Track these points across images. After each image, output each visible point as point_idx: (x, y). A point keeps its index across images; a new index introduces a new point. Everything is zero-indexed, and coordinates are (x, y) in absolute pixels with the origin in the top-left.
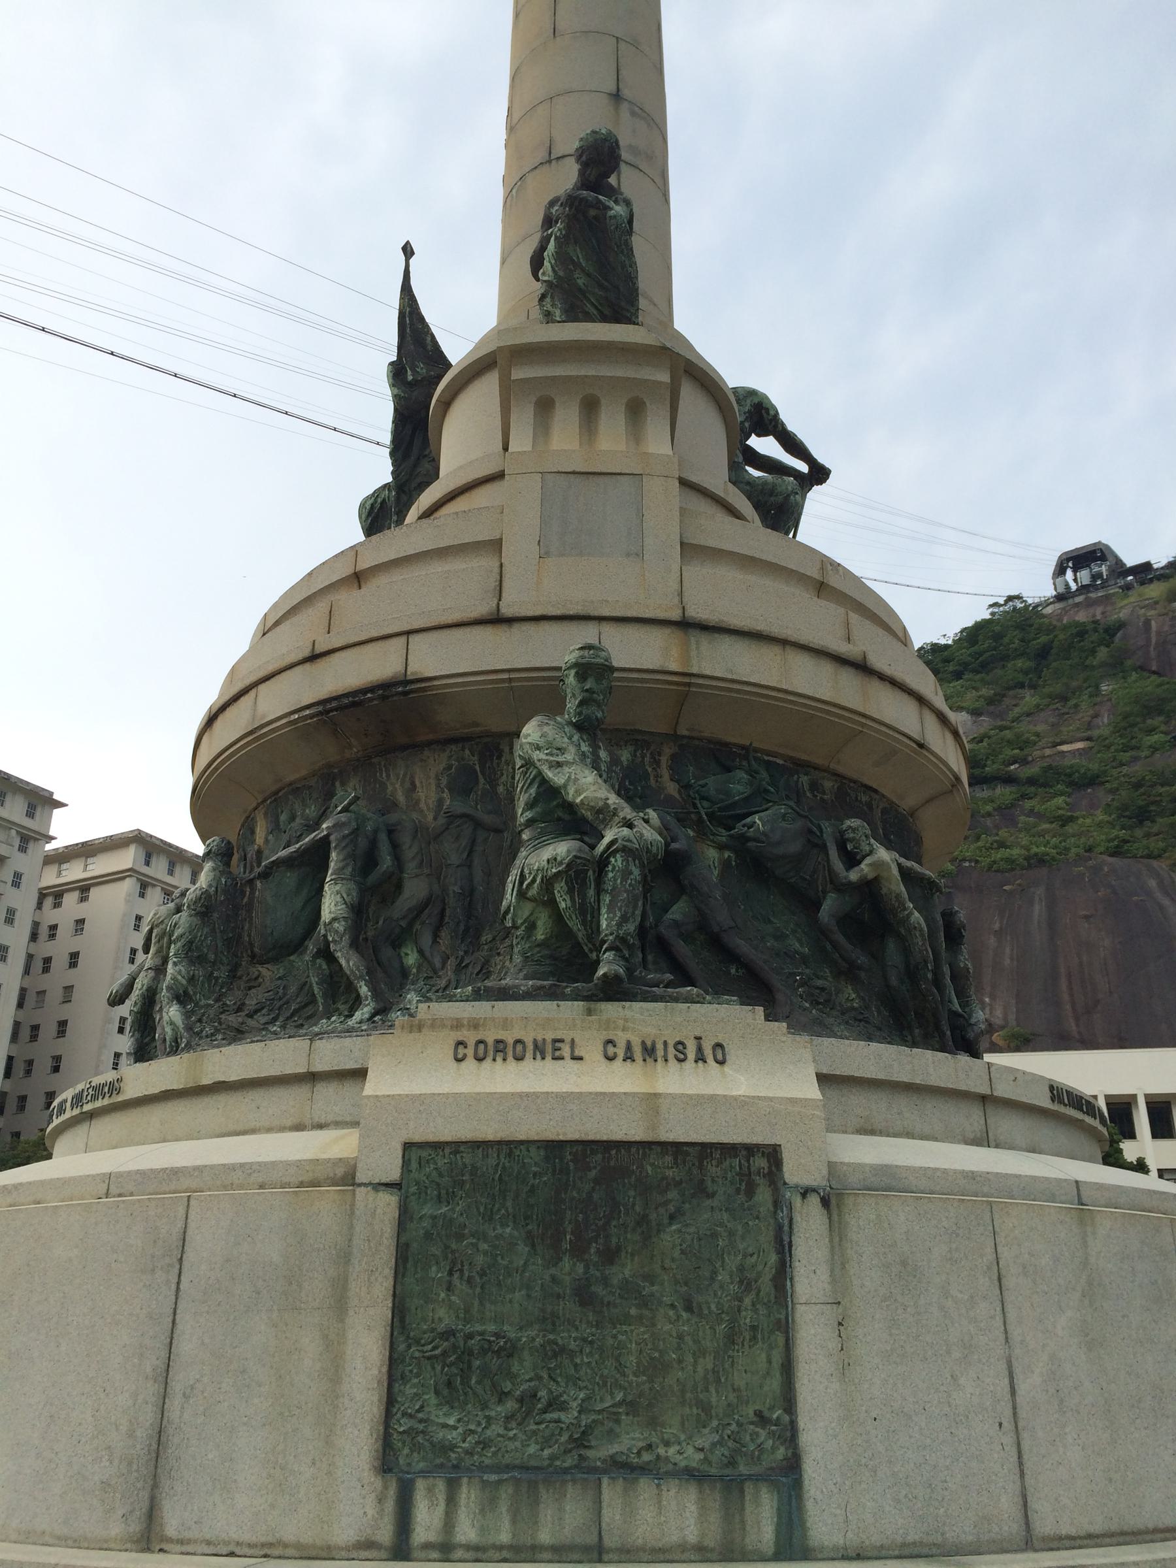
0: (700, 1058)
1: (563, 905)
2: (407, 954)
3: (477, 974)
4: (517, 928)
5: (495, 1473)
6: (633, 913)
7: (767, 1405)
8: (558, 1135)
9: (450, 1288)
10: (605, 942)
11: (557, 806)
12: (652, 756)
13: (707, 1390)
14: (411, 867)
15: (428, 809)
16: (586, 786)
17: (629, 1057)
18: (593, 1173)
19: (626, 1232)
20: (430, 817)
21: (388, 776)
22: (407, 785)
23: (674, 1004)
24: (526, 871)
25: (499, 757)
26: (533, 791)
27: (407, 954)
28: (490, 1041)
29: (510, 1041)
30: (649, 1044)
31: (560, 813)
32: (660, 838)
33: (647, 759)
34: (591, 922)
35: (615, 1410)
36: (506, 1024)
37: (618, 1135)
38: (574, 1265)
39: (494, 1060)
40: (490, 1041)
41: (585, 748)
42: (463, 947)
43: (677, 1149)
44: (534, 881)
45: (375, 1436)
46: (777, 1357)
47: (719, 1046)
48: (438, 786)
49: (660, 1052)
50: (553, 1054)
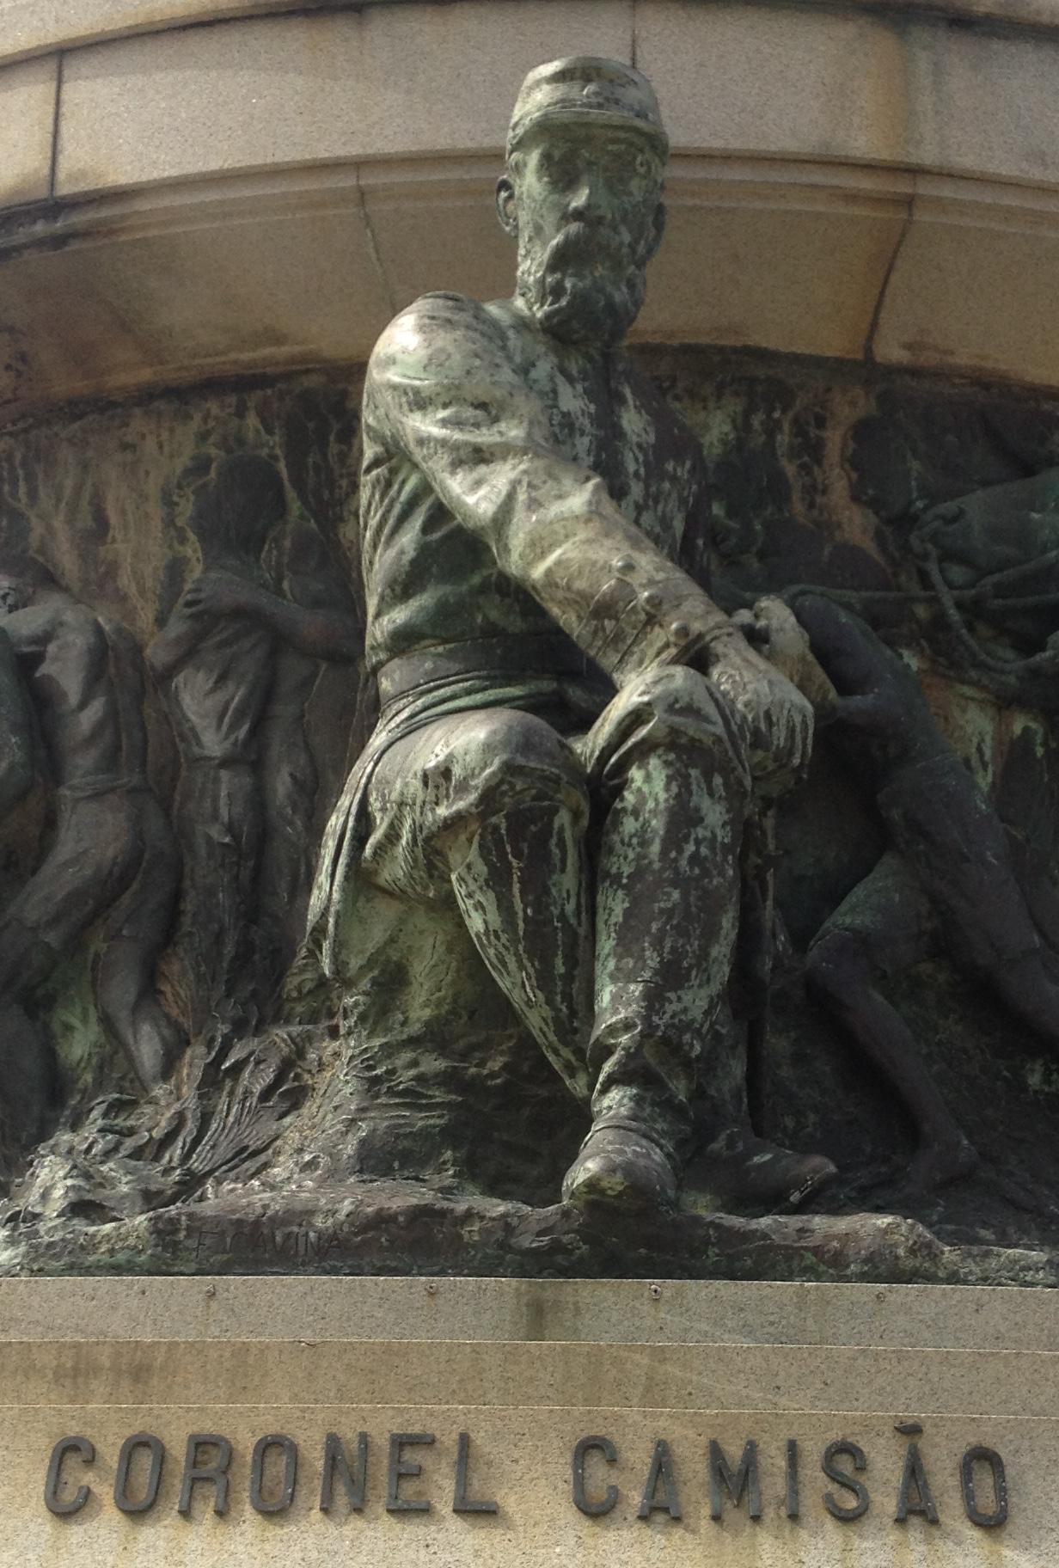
0: (917, 1508)
1: (476, 923)
2: (69, 1028)
3: (265, 1095)
4: (348, 984)
6: (703, 955)
10: (609, 1051)
11: (483, 589)
12: (799, 428)
14: (82, 765)
15: (142, 592)
16: (561, 533)
17: (661, 1508)
20: (146, 616)
21: (33, 495)
22: (86, 521)
24: (375, 804)
26: (409, 539)
27: (69, 1028)
29: (246, 1443)
30: (734, 1451)
31: (493, 611)
32: (798, 698)
33: (783, 439)
34: (568, 978)
36: (242, 1370)
41: (572, 401)
42: (231, 1010)
47: (982, 1458)
48: (170, 522)
49: (773, 1483)
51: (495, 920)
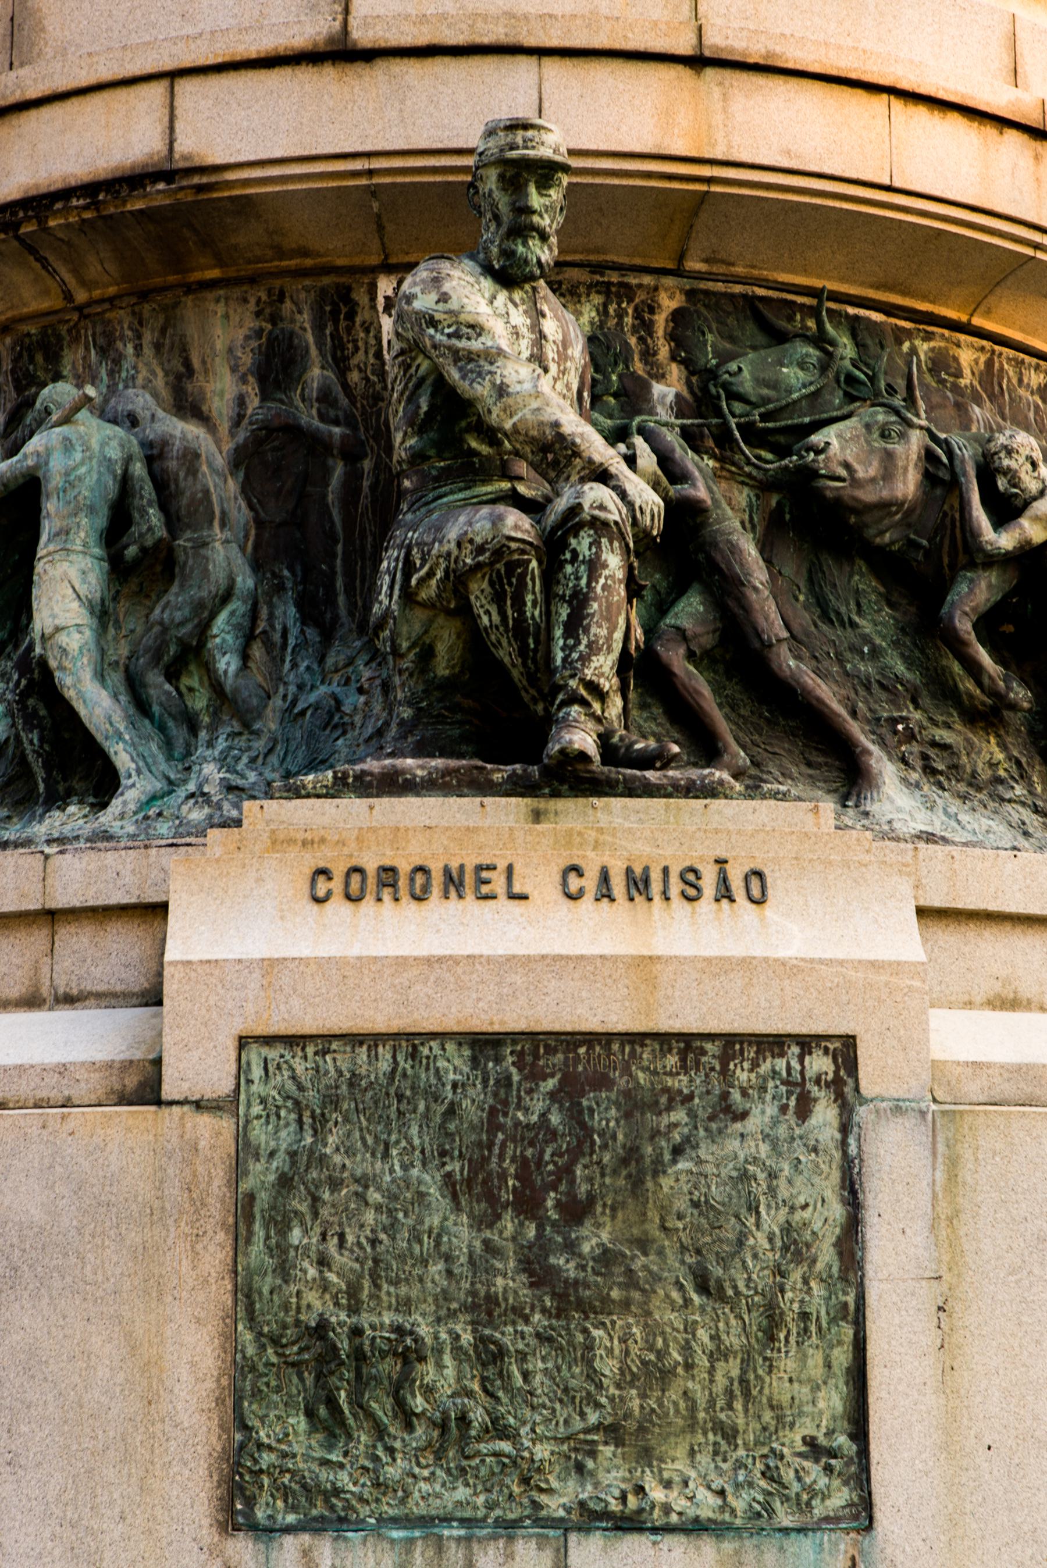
0: (725, 893)
5: (405, 1528)
7: (824, 1430)
8: (492, 1023)
9: (323, 1262)
12: (638, 315)
13: (730, 1407)
17: (605, 893)
18: (551, 1084)
19: (603, 1175)
23: (682, 802)
25: (351, 316)
28: (371, 867)
30: (638, 870)
33: (629, 320)
35: (589, 1437)
37: (592, 1023)
38: (521, 1224)
39: (379, 900)
40: (371, 867)
43: (688, 1044)
44: (431, 574)
45: (215, 1478)
46: (842, 1357)
49: (656, 887)
50: (477, 889)
51: (496, 618)
